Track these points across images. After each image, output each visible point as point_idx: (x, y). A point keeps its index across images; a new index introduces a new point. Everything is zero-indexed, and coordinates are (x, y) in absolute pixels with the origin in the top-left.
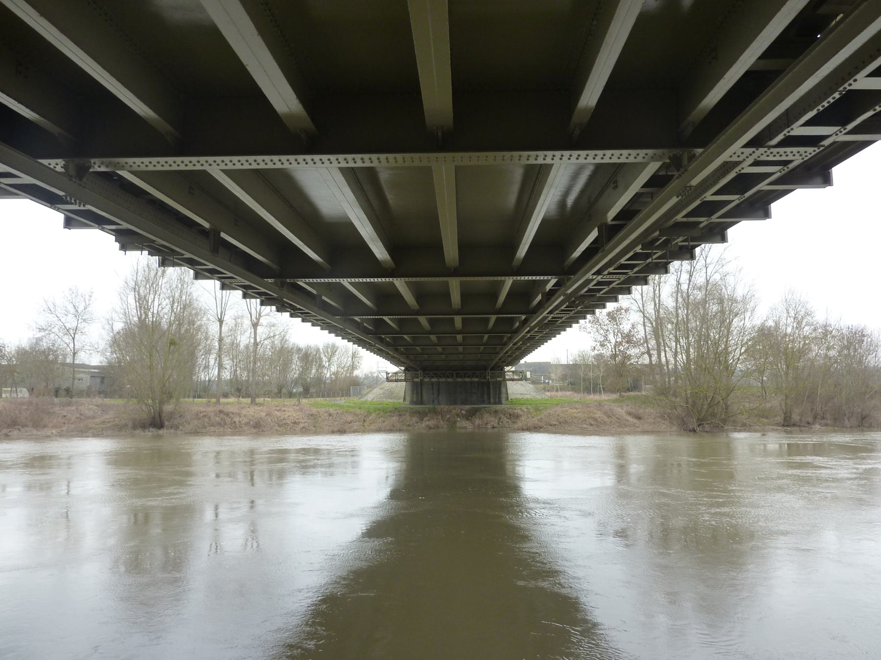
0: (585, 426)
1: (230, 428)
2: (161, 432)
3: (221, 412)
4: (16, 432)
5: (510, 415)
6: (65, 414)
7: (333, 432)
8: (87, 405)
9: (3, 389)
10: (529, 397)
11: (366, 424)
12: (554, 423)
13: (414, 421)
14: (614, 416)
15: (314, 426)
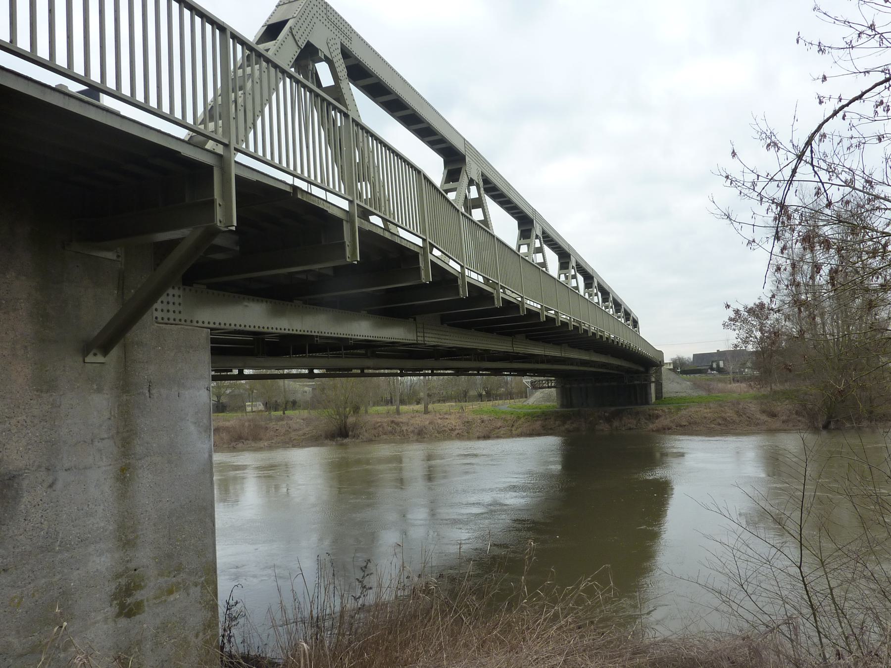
0: (713, 426)
1: (399, 436)
2: (346, 441)
3: (393, 422)
4: (240, 445)
5: (650, 415)
6: (278, 429)
7: (479, 438)
8: (296, 419)
9: (247, 404)
10: (684, 395)
11: (513, 429)
12: (684, 424)
13: (557, 425)
14: (745, 414)
15: (467, 433)
